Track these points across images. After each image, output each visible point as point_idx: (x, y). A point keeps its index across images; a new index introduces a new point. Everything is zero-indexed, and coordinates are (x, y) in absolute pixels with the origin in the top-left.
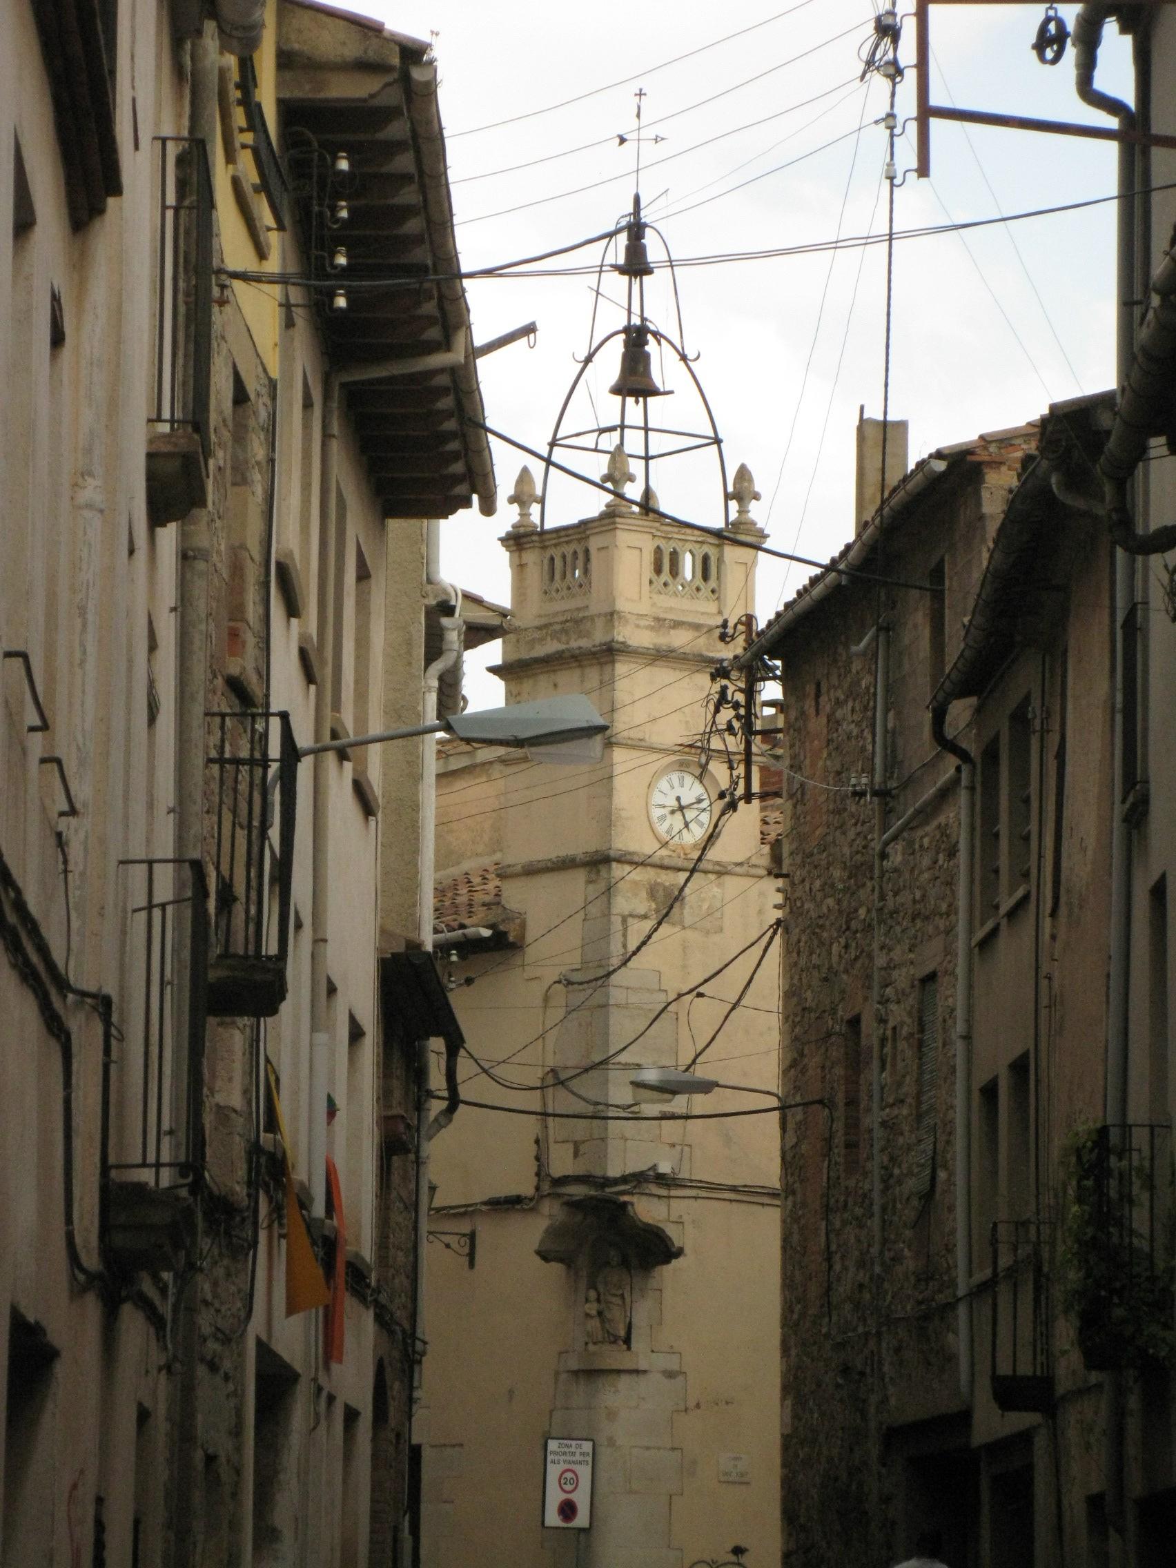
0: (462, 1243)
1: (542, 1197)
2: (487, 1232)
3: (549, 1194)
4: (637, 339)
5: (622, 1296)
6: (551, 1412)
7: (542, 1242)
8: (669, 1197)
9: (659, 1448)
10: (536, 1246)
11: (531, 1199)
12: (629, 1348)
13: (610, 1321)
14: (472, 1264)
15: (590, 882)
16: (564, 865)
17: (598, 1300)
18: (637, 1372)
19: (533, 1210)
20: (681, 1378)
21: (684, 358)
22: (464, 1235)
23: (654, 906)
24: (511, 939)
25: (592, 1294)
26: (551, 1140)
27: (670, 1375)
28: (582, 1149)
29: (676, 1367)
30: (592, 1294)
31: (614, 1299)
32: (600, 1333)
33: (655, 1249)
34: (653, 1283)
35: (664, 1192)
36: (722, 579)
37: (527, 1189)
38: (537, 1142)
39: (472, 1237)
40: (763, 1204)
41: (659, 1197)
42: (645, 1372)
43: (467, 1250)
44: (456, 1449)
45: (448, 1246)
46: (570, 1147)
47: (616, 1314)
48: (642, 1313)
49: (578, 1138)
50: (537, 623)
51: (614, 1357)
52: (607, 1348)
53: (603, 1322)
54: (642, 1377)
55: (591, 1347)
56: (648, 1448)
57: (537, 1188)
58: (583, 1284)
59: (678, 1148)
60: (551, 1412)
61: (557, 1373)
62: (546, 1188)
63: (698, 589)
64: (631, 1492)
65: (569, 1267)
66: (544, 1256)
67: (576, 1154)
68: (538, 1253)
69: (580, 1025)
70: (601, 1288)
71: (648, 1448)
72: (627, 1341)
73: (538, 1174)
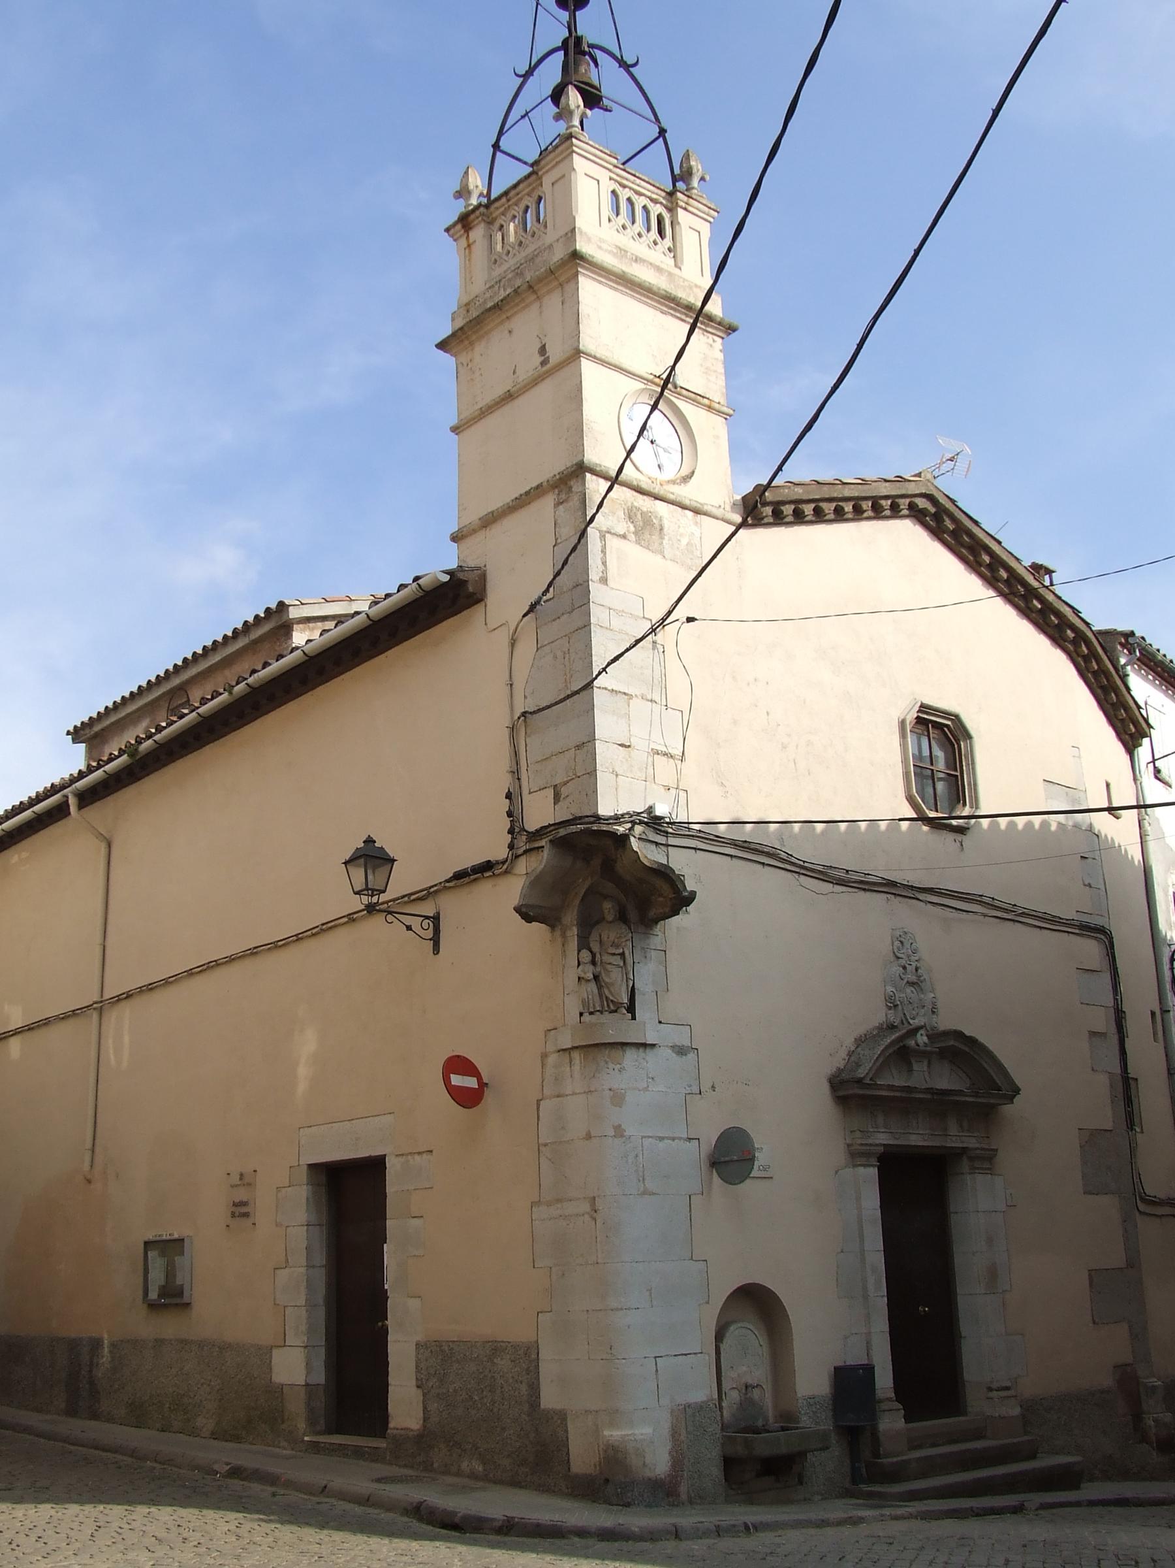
0: (425, 926)
1: (517, 857)
2: (452, 906)
3: (525, 852)
4: (575, 49)
5: (622, 955)
6: (538, 1101)
7: (523, 896)
8: (668, 845)
9: (673, 1139)
10: (516, 902)
11: (504, 862)
12: (634, 1018)
13: (608, 985)
14: (436, 949)
15: (558, 504)
16: (537, 492)
17: (593, 963)
18: (645, 1045)
19: (506, 872)
20: (691, 1056)
21: (622, 63)
22: (427, 917)
23: (632, 529)
24: (471, 589)
25: (586, 955)
26: (525, 792)
27: (681, 1051)
28: (564, 791)
29: (687, 1043)
30: (586, 955)
31: (612, 959)
32: (597, 999)
33: (659, 896)
34: (656, 941)
35: (661, 839)
36: (678, 238)
37: (500, 852)
38: (509, 796)
39: (436, 919)
40: (763, 864)
41: (657, 844)
42: (653, 1046)
43: (430, 934)
44: (425, 1156)
45: (409, 928)
46: (550, 793)
47: (614, 976)
48: (645, 976)
49: (558, 780)
50: (484, 288)
51: (615, 1028)
52: (607, 1018)
53: (600, 988)
54: (650, 1054)
55: (587, 1018)
56: (661, 1139)
57: (511, 847)
58: (573, 944)
59: (673, 791)
60: (538, 1101)
61: (544, 1056)
62: (522, 843)
63: (655, 243)
64: (644, 1193)
65: (553, 927)
66: (526, 913)
67: (557, 798)
68: (517, 910)
69: (555, 657)
70: (595, 947)
71: (661, 1139)
72: (631, 1009)
73: (511, 831)
